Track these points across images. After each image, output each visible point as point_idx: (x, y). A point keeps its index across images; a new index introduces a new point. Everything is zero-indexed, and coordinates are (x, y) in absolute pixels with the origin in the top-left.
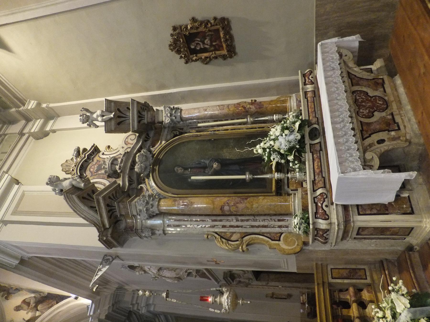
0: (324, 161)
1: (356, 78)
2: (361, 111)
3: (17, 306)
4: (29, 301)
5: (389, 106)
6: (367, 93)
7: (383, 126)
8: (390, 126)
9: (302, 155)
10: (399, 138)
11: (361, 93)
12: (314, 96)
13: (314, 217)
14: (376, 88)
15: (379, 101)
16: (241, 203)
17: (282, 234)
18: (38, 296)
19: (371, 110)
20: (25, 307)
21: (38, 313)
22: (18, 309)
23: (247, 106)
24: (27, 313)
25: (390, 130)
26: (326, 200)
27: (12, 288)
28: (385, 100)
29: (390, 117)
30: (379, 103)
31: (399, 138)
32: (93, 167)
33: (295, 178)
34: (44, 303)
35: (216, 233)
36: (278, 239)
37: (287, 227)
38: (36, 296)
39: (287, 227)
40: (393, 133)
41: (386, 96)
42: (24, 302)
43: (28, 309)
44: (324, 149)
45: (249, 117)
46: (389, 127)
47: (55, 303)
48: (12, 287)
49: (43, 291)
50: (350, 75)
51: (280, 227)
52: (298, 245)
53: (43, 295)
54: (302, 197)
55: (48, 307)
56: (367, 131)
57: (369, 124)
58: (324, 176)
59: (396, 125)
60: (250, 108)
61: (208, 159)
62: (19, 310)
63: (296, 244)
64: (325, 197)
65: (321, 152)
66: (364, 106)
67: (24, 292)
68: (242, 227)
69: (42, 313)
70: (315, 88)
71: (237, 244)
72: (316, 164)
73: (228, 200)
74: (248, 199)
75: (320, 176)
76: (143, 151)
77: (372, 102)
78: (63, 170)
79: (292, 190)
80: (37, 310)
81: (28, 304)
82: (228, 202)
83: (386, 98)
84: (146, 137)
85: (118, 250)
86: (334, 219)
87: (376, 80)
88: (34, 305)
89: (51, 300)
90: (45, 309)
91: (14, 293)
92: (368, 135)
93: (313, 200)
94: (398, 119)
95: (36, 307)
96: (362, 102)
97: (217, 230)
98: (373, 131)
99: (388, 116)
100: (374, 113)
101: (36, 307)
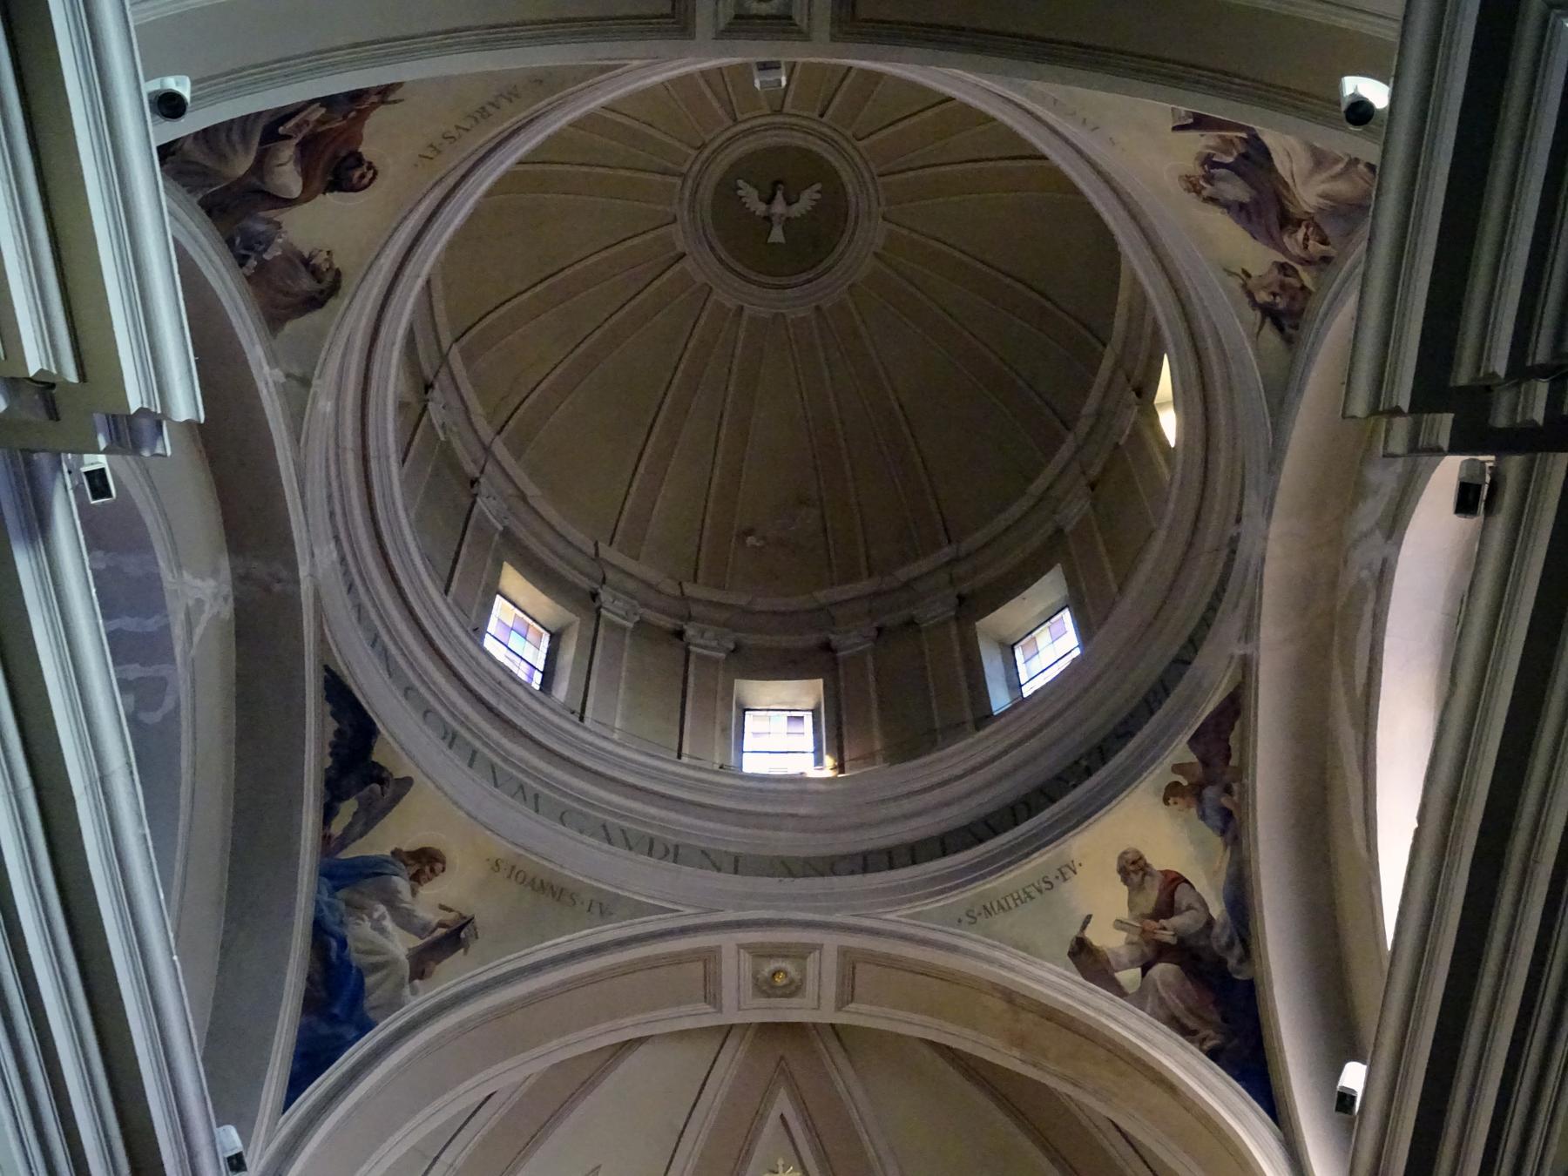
3: (1141, 858)
4: (1184, 904)
9: (492, 590)
18: (1221, 936)
20: (1151, 896)
21: (1129, 977)
22: (1133, 868)
24: (1120, 924)
27: (1228, 790)
34: (1189, 985)
38: (1217, 930)
42: (1174, 881)
43: (1144, 916)
47: (1209, 1044)
48: (1235, 787)
49: (1255, 955)
53: (1232, 962)
55: (1177, 1014)
62: (1125, 880)
67: (1222, 859)
80: (1145, 969)
81: (1166, 908)
88: (1167, 937)
89: (1216, 1018)
90: (1162, 1001)
91: (1203, 817)
95: (1161, 952)
101: (1161, 952)
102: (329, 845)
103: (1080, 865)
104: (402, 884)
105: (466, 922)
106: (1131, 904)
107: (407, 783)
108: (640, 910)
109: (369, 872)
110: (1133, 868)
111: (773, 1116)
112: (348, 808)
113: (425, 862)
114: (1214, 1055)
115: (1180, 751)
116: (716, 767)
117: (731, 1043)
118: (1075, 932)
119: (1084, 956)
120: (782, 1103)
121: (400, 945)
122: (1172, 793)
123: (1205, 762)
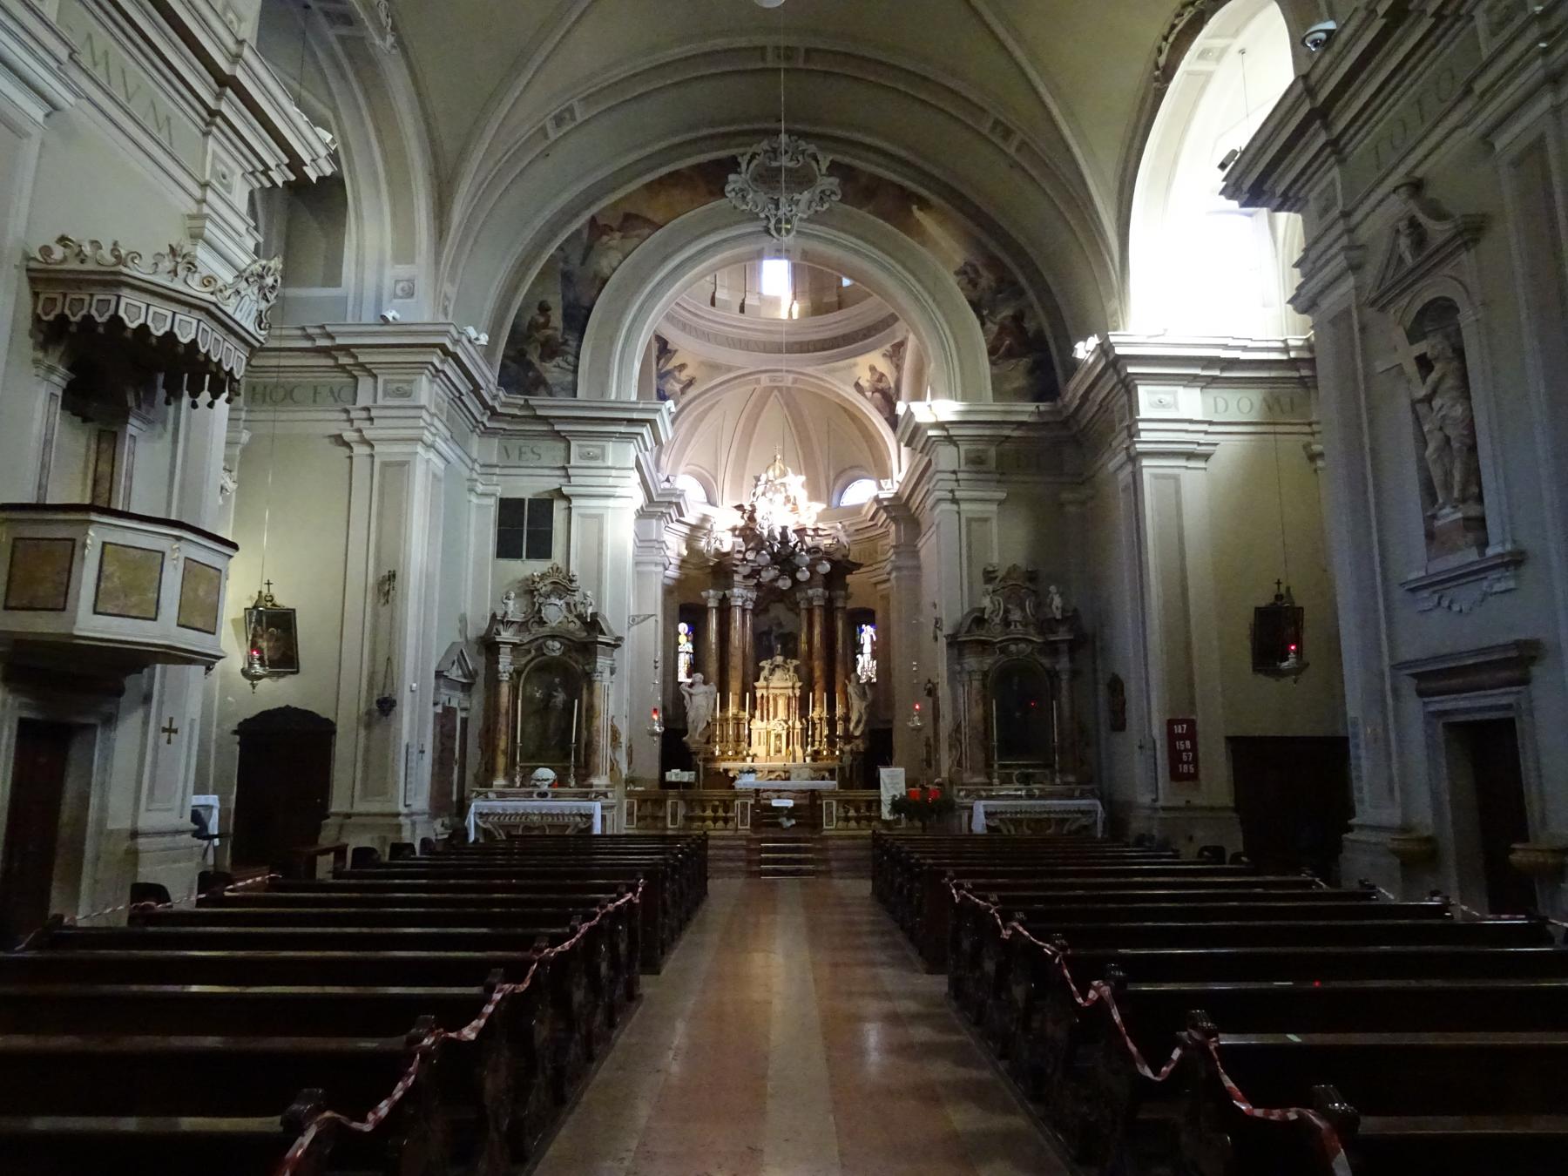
18: (893, 391)
20: (876, 377)
21: (869, 394)
22: (873, 369)
42: (882, 375)
45: (756, 684)
61: (506, 604)
67: (895, 374)
69: (870, 400)
76: (1190, 1035)
85: (943, 642)
86: (965, 801)
88: (880, 387)
102: (658, 370)
103: (1242, 52)
104: (677, 373)
105: (694, 378)
106: (872, 377)
107: (676, 351)
108: (739, 368)
109: (669, 373)
110: (873, 369)
112: (662, 361)
113: (682, 367)
114: (886, 419)
115: (888, 347)
116: (408, 803)
118: (855, 380)
119: (857, 386)
121: (677, 387)
122: (884, 355)
123: (894, 351)
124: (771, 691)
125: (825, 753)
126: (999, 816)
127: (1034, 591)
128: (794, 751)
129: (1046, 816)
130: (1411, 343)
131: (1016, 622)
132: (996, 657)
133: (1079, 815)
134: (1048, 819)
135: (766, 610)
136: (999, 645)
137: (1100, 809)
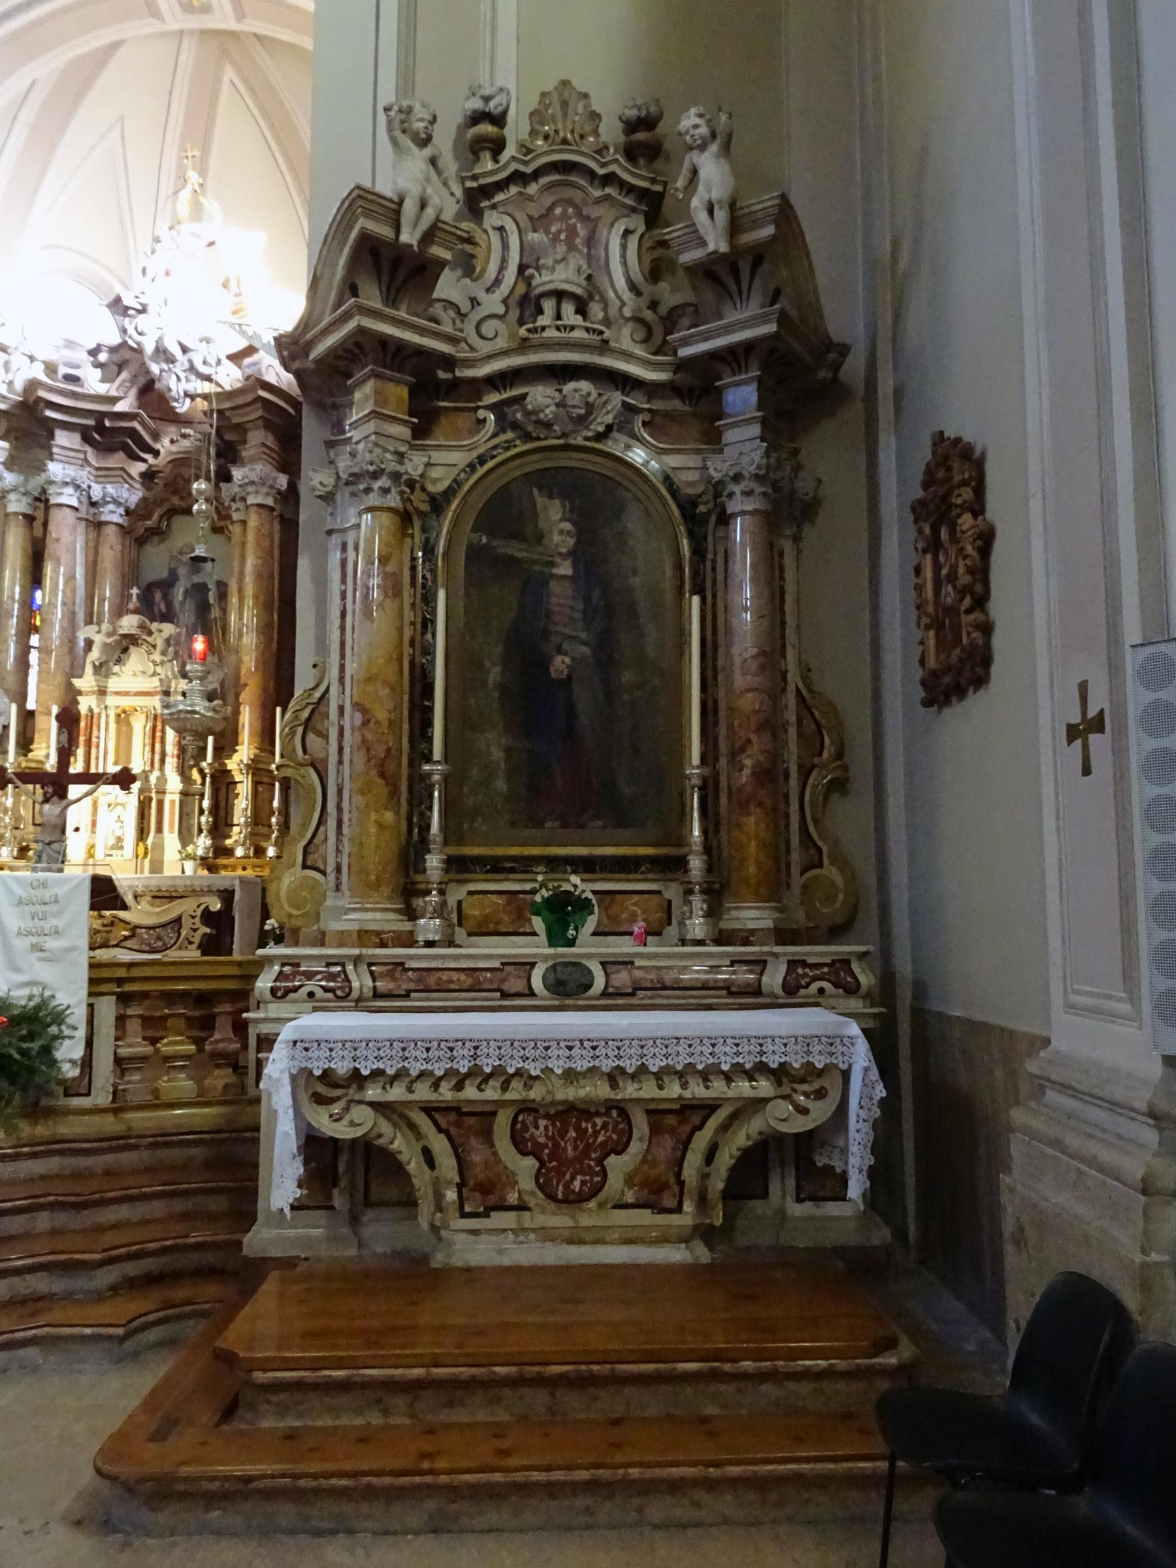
0: (465, 1000)
1: (687, 1128)
2: (542, 1123)
5: (560, 1208)
6: (619, 1153)
7: (479, 1173)
8: (478, 1195)
10: (440, 1208)
11: (621, 1133)
12: (733, 989)
13: (736, 958)
14: (636, 1180)
15: (583, 1183)
16: (369, 761)
17: (324, 873)
19: (546, 1151)
23: (750, 756)
25: (464, 1190)
26: (330, 995)
28: (589, 1199)
29: (512, 1198)
30: (573, 1178)
31: (440, 1208)
32: (570, 210)
33: (691, 912)
35: (327, 690)
36: (309, 863)
37: (338, 888)
39: (338, 888)
40: (451, 1195)
41: (601, 1205)
44: (507, 1003)
45: (77, 682)
46: (474, 1190)
50: (703, 1113)
51: (338, 869)
52: (290, 916)
54: (366, 931)
56: (458, 1125)
57: (487, 1135)
58: (413, 995)
59: (482, 1209)
60: (741, 770)
63: (295, 912)
64: (339, 993)
65: (498, 994)
66: (563, 1133)
68: (340, 762)
70: (773, 995)
71: (294, 750)
72: (455, 976)
73: (377, 722)
74: (380, 781)
75: (412, 986)
77: (579, 1159)
78: (544, 95)
79: (460, 903)
82: (372, 724)
83: (592, 1204)
84: (691, 389)
87: (676, 1189)
92: (444, 1125)
93: (613, 959)
94: (501, 1219)
96: (581, 1133)
97: (334, 691)
98: (457, 1141)
99: (516, 1195)
100: (605, 1162)
111: (226, 86)
117: (186, 42)
120: (229, 73)
124: (111, 700)
125: (239, 852)
126: (373, 1093)
127: (643, 195)
128: (159, 847)
129: (601, 1090)
130: (1103, 733)
131: (560, 295)
132: (483, 439)
133: (764, 1087)
134: (620, 1109)
135: (158, 533)
136: (493, 398)
137: (861, 1056)
